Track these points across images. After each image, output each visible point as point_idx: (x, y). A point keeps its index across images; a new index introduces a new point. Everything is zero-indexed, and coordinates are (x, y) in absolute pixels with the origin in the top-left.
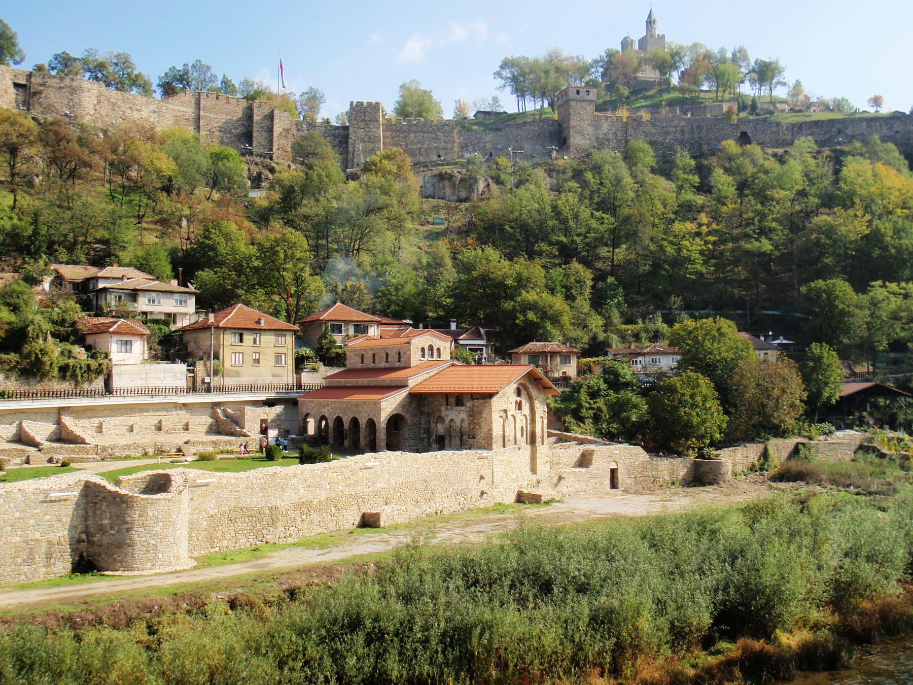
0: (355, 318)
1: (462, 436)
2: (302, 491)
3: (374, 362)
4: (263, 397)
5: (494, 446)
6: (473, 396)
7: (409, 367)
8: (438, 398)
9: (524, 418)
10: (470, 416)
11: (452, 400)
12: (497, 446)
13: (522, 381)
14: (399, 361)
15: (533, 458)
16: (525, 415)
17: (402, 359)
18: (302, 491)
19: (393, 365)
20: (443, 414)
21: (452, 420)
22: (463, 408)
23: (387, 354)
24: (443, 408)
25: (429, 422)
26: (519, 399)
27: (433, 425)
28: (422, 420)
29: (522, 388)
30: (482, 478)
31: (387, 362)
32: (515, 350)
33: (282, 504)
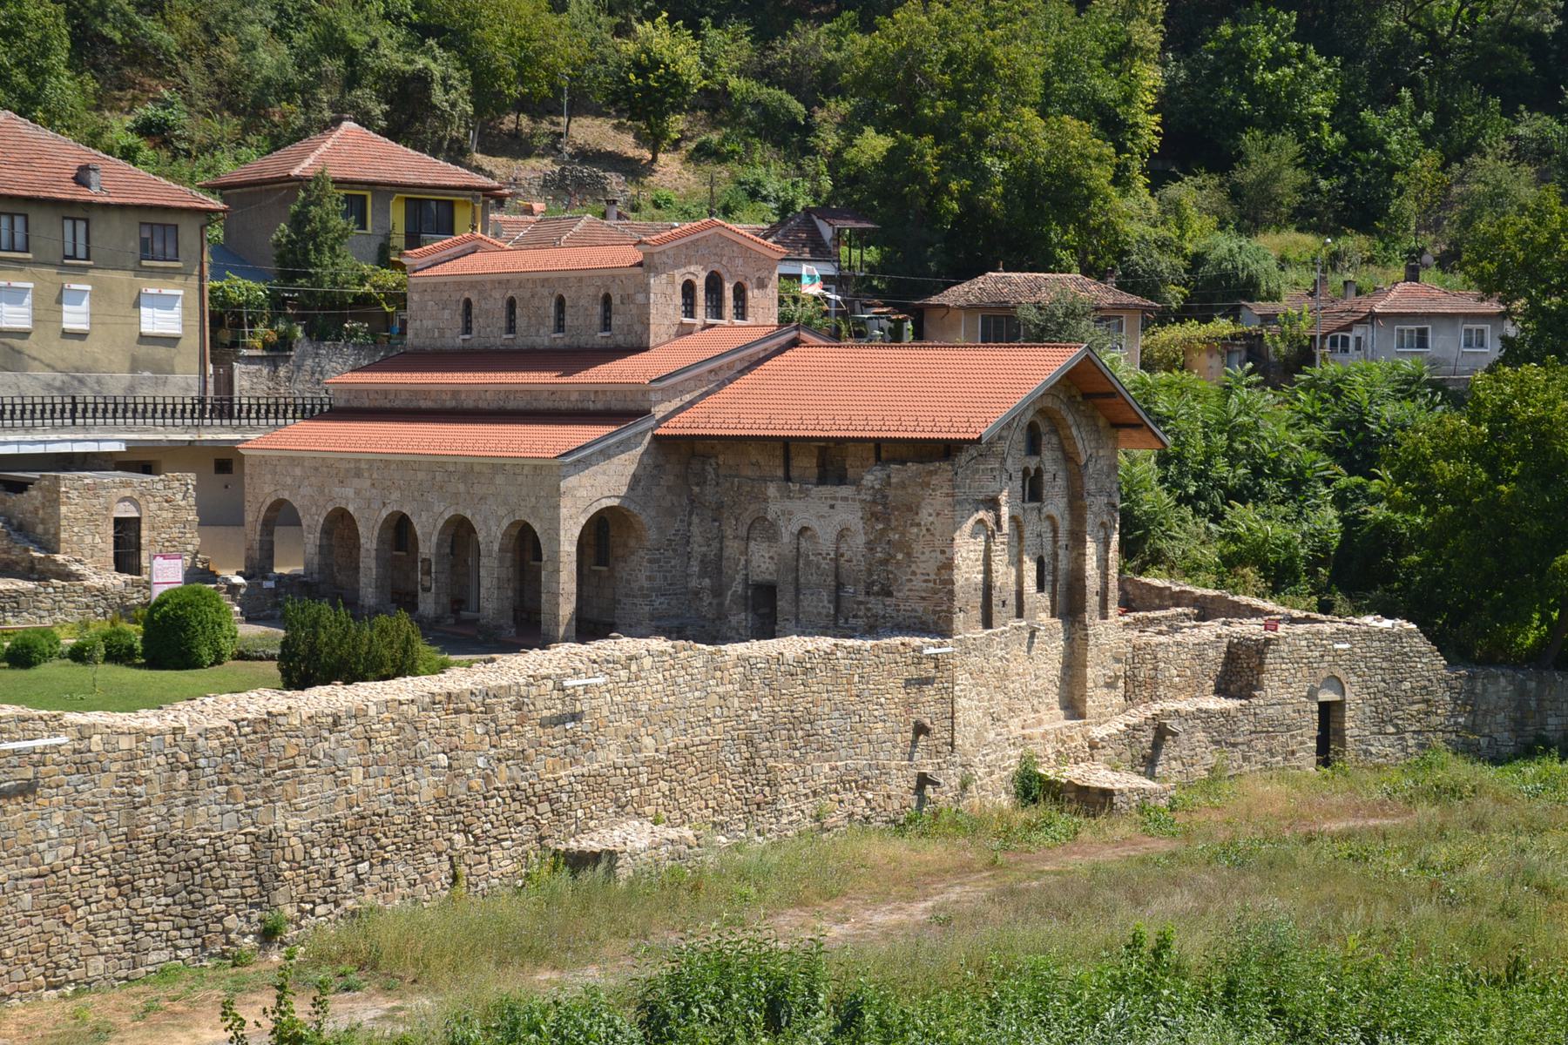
0: (411, 178)
1: (839, 586)
2: (357, 775)
3: (511, 328)
4: (113, 443)
5: (959, 620)
6: (887, 451)
7: (646, 349)
8: (851, 447)
9: (1045, 527)
10: (875, 516)
11: (806, 464)
12: (967, 627)
13: (1048, 403)
14: (606, 326)
15: (1073, 667)
16: (1050, 518)
17: (616, 321)
18: (357, 775)
19: (584, 340)
20: (773, 510)
21: (804, 530)
22: (845, 491)
23: (560, 302)
24: (772, 490)
25: (722, 539)
26: (1032, 463)
27: (732, 547)
28: (695, 530)
29: (1044, 427)
30: (921, 729)
31: (560, 327)
32: (934, 300)
33: (294, 823)
